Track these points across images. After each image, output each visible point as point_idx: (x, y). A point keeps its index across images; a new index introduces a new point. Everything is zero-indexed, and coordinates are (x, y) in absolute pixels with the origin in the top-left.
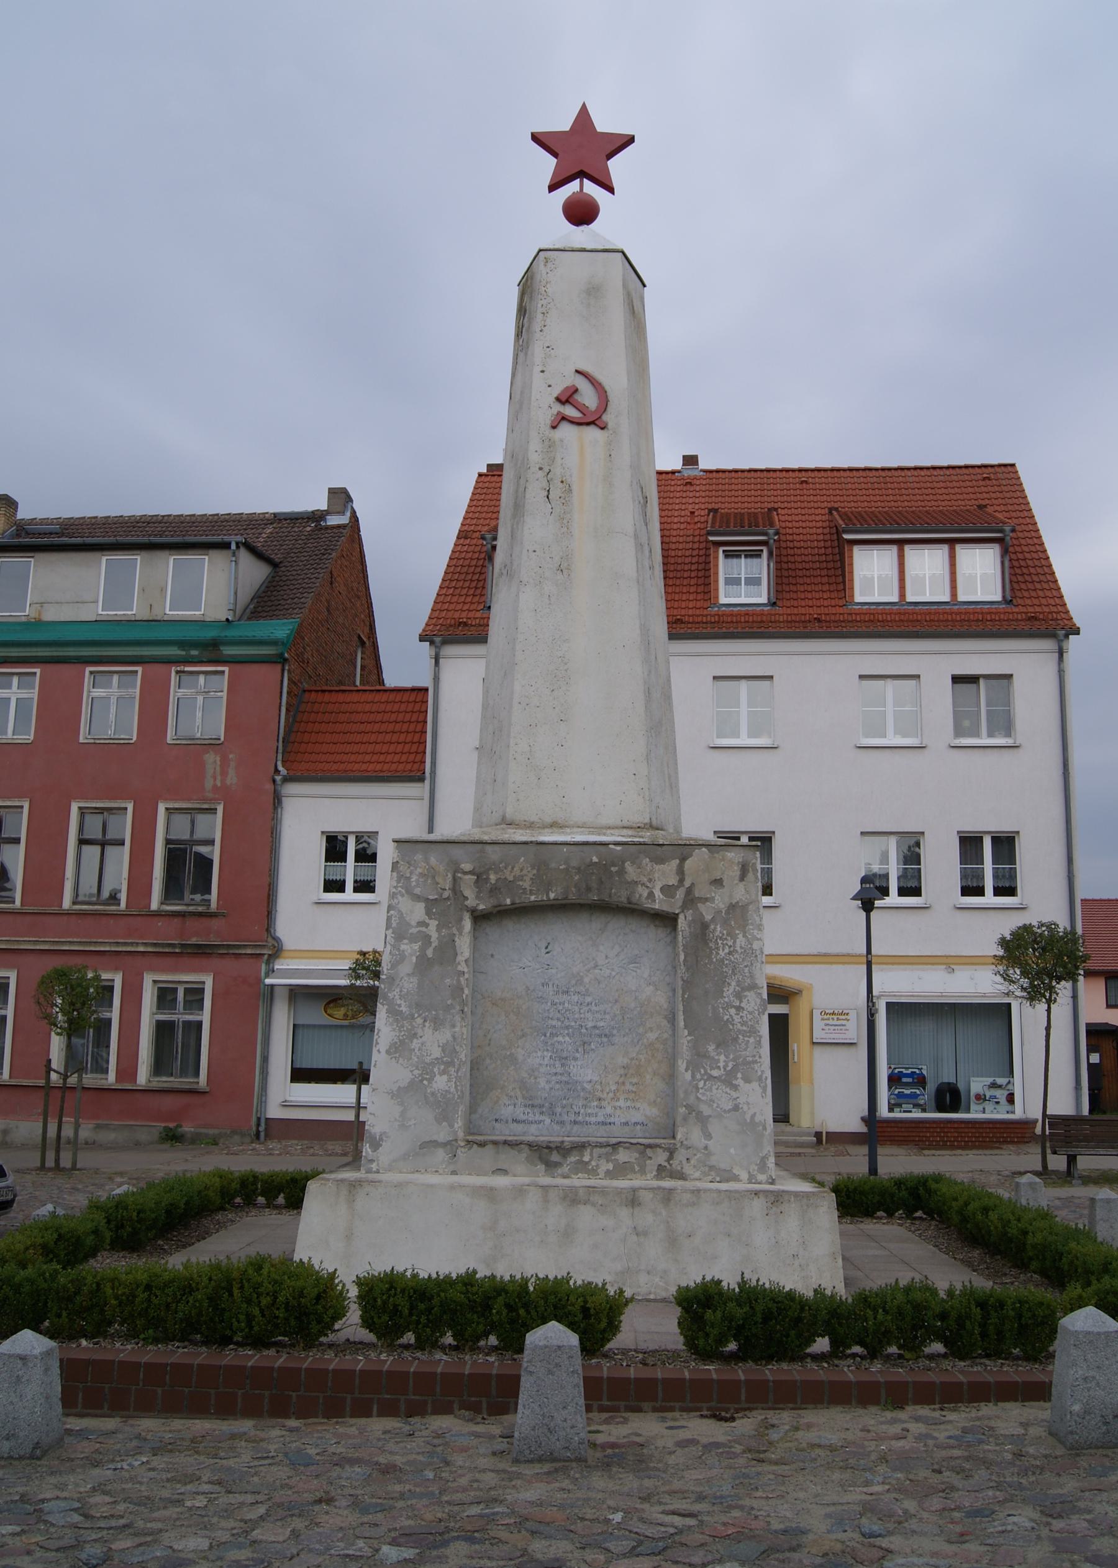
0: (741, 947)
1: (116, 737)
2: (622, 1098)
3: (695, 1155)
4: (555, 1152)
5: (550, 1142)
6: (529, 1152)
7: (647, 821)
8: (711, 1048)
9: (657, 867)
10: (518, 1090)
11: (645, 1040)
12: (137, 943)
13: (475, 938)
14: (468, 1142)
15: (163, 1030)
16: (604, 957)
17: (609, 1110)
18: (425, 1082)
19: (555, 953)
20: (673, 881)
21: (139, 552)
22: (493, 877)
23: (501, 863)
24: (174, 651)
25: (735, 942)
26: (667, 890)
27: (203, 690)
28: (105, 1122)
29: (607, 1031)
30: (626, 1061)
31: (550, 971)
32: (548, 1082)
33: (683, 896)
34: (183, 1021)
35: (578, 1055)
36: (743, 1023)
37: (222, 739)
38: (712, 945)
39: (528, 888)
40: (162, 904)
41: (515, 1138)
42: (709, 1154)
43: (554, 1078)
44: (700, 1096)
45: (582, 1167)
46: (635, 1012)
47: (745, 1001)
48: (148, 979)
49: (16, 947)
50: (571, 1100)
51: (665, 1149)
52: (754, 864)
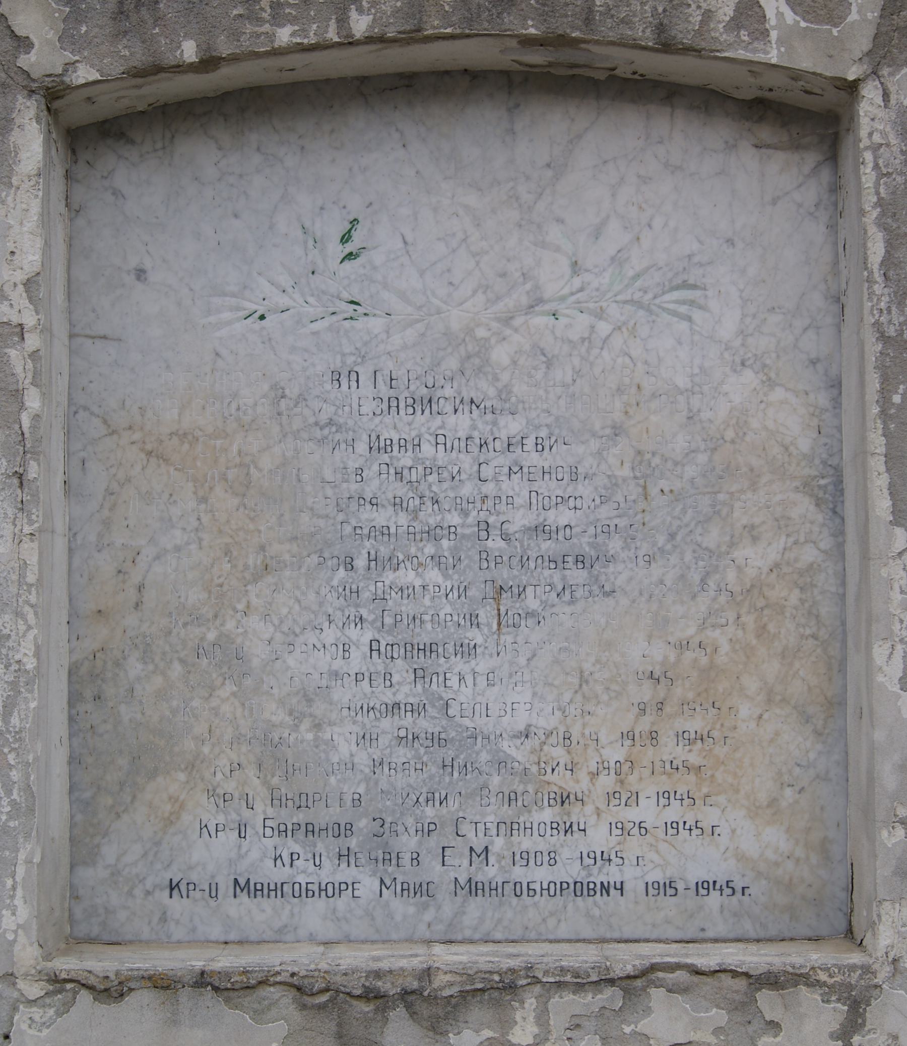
2: (649, 790)
4: (398, 1014)
6: (297, 1016)
10: (251, 772)
11: (731, 575)
13: (73, 209)
14: (57, 982)
16: (564, 265)
19: (378, 257)
29: (584, 544)
30: (659, 652)
31: (359, 324)
33: (872, 15)
35: (476, 636)
43: (386, 723)
46: (690, 471)
50: (453, 804)
51: (829, 991)
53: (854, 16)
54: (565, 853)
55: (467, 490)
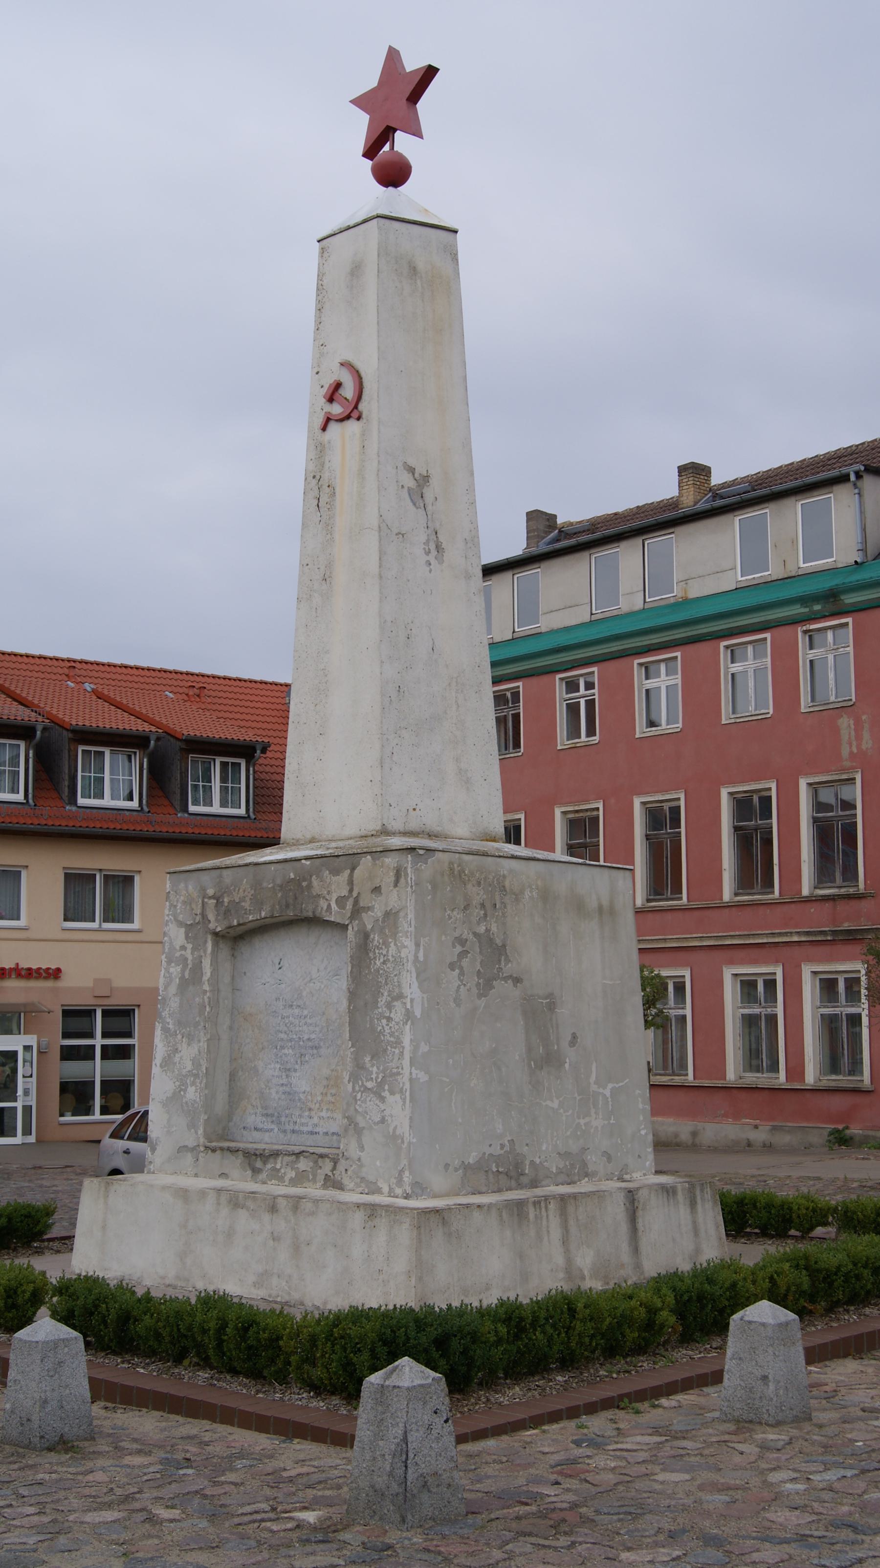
0: (393, 956)
1: (758, 712)
3: (351, 1166)
4: (259, 1159)
5: (256, 1149)
7: (379, 828)
8: (367, 1059)
9: (334, 879)
12: (791, 933)
14: (206, 1147)
15: (830, 1024)
17: (315, 1120)
18: (182, 1093)
20: (345, 893)
21: (766, 505)
22: (226, 900)
23: (231, 886)
24: (797, 610)
25: (388, 951)
26: (341, 901)
27: (832, 647)
28: (780, 1124)
32: (277, 1092)
33: (351, 907)
34: (847, 1015)
36: (392, 1034)
37: (854, 700)
38: (371, 955)
39: (248, 908)
40: (815, 888)
41: (255, 1146)
42: (361, 1166)
43: (281, 1089)
44: (357, 1107)
45: (276, 1175)
47: (393, 1011)
48: (806, 971)
49: (788, 940)
50: (291, 1110)
52: (406, 868)
53: (348, 908)
54: (310, 1124)
55: (297, 1029)
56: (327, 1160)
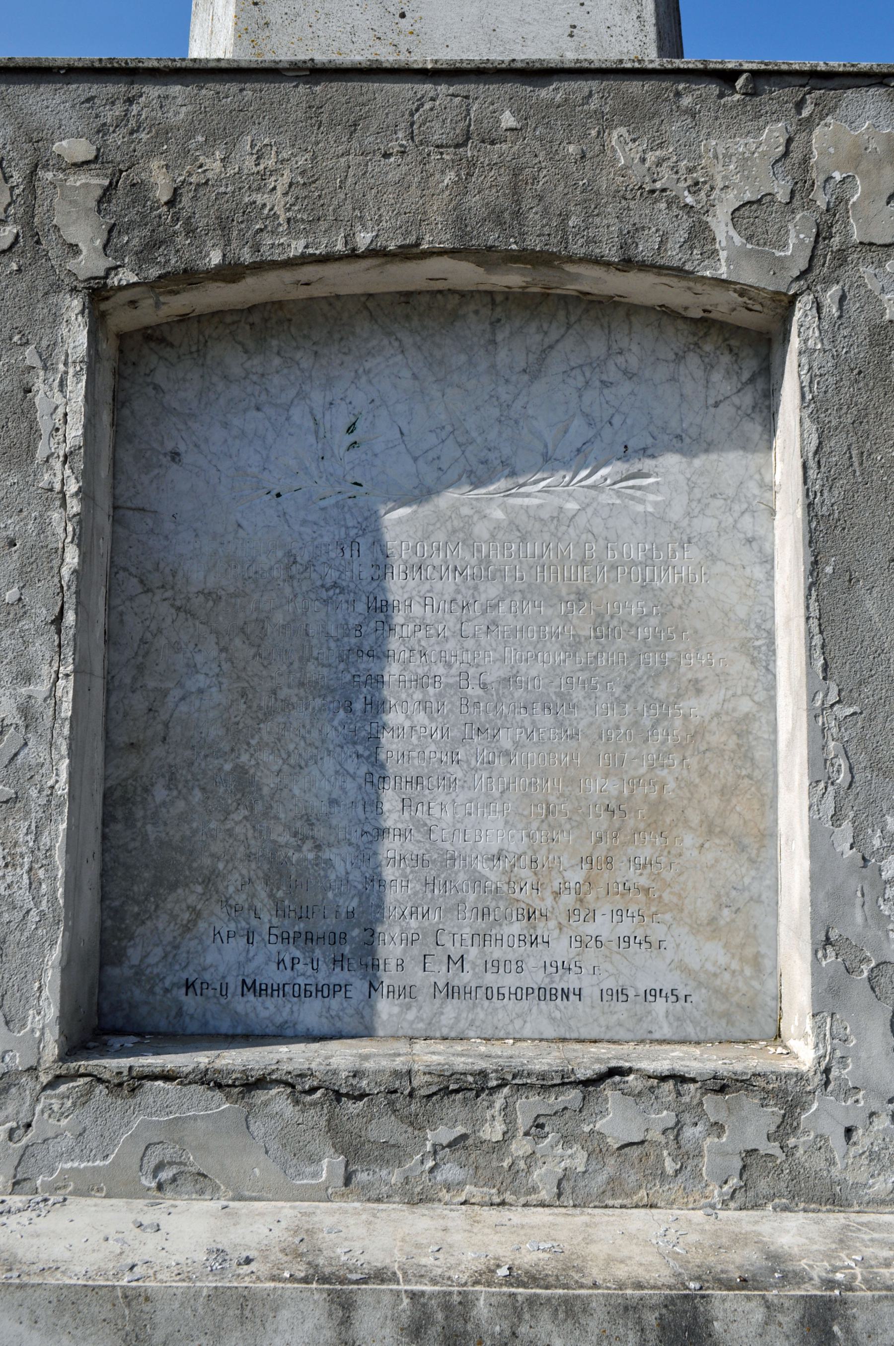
2: (604, 909)
17: (561, 949)
56: (750, 1102)
